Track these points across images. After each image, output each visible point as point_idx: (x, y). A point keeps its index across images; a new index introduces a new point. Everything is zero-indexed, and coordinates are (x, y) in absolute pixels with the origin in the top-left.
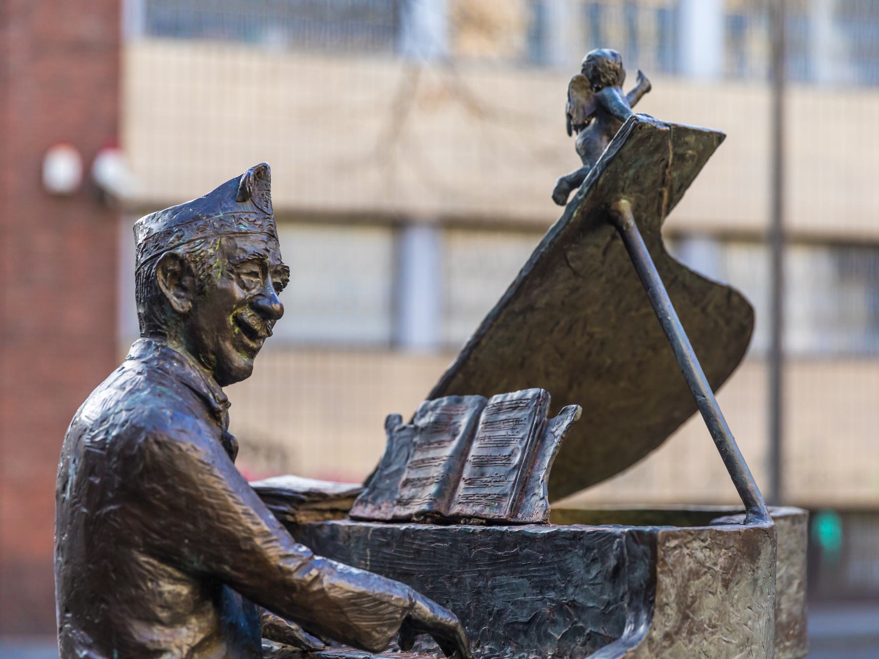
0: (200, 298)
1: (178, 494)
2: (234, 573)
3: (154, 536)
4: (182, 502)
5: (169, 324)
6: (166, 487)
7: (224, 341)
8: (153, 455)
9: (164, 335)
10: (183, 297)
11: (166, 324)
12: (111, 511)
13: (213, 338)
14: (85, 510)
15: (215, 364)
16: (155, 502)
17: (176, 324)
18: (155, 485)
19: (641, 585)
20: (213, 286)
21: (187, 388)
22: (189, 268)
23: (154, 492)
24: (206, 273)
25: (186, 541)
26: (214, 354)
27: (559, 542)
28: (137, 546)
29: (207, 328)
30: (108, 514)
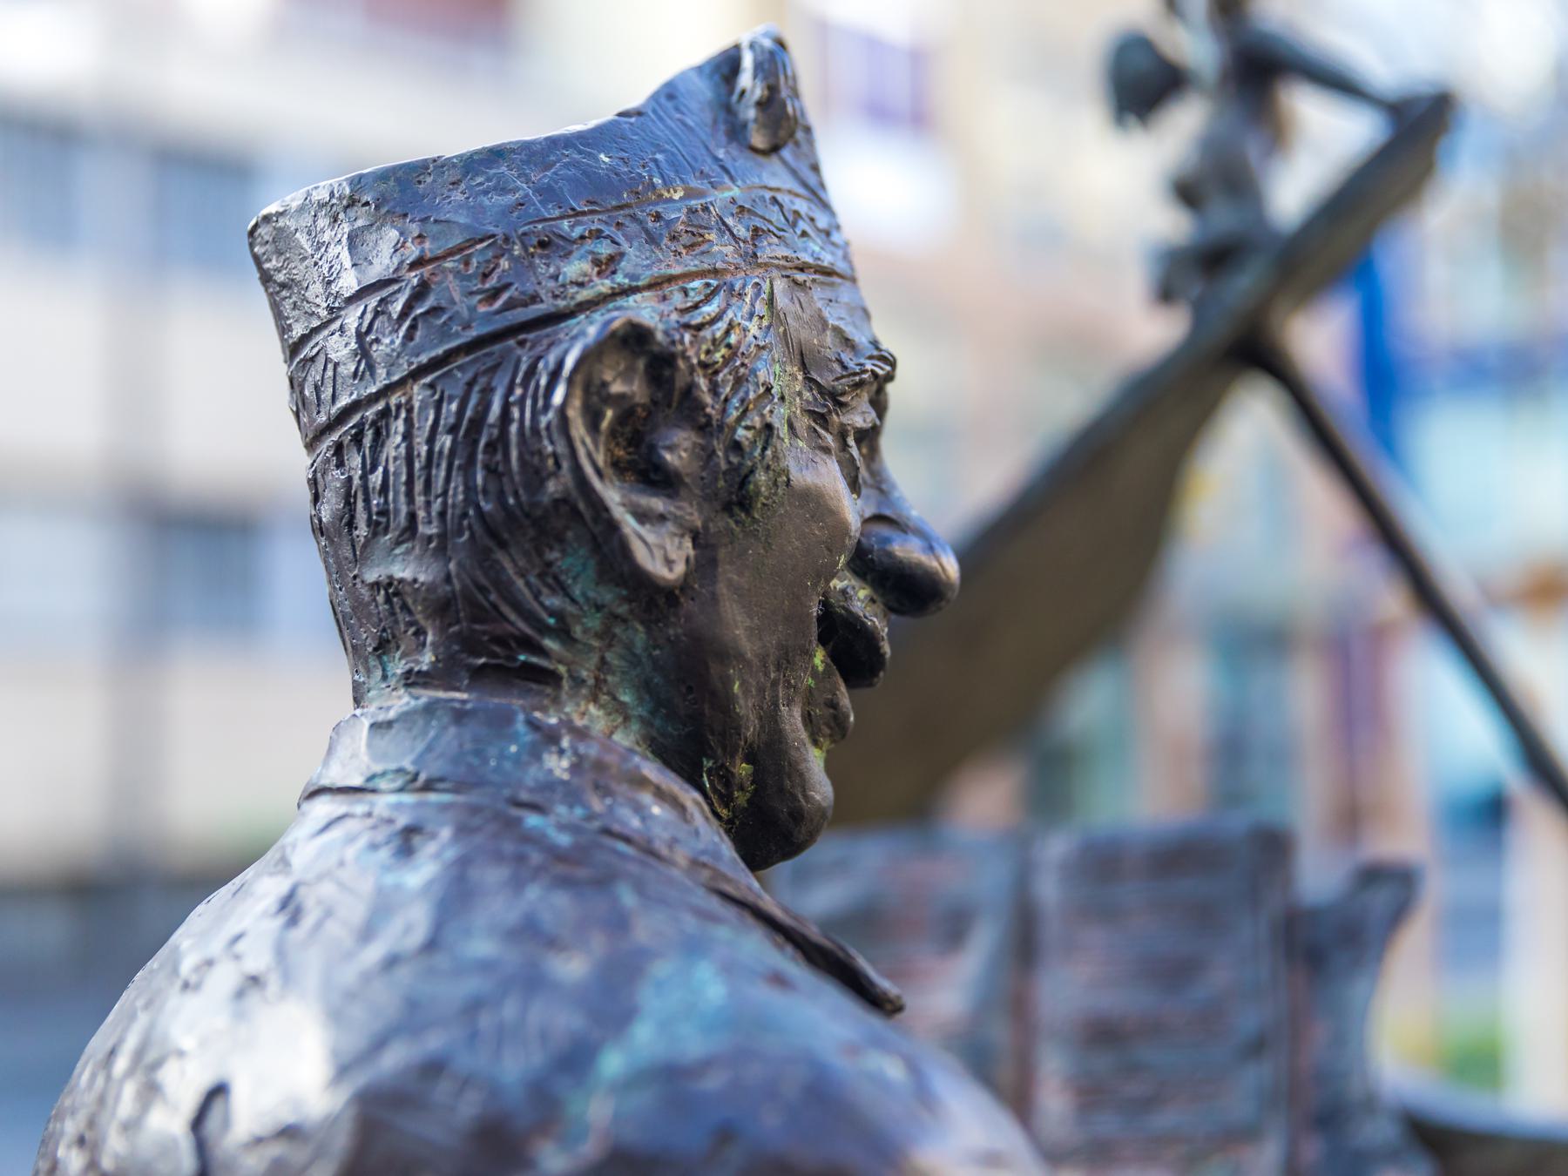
0: (723, 522)
5: (577, 631)
9: (546, 677)
10: (662, 518)
11: (563, 632)
13: (761, 690)
15: (741, 799)
17: (606, 635)
20: (781, 478)
22: (691, 388)
24: (757, 422)
26: (750, 758)
29: (748, 647)
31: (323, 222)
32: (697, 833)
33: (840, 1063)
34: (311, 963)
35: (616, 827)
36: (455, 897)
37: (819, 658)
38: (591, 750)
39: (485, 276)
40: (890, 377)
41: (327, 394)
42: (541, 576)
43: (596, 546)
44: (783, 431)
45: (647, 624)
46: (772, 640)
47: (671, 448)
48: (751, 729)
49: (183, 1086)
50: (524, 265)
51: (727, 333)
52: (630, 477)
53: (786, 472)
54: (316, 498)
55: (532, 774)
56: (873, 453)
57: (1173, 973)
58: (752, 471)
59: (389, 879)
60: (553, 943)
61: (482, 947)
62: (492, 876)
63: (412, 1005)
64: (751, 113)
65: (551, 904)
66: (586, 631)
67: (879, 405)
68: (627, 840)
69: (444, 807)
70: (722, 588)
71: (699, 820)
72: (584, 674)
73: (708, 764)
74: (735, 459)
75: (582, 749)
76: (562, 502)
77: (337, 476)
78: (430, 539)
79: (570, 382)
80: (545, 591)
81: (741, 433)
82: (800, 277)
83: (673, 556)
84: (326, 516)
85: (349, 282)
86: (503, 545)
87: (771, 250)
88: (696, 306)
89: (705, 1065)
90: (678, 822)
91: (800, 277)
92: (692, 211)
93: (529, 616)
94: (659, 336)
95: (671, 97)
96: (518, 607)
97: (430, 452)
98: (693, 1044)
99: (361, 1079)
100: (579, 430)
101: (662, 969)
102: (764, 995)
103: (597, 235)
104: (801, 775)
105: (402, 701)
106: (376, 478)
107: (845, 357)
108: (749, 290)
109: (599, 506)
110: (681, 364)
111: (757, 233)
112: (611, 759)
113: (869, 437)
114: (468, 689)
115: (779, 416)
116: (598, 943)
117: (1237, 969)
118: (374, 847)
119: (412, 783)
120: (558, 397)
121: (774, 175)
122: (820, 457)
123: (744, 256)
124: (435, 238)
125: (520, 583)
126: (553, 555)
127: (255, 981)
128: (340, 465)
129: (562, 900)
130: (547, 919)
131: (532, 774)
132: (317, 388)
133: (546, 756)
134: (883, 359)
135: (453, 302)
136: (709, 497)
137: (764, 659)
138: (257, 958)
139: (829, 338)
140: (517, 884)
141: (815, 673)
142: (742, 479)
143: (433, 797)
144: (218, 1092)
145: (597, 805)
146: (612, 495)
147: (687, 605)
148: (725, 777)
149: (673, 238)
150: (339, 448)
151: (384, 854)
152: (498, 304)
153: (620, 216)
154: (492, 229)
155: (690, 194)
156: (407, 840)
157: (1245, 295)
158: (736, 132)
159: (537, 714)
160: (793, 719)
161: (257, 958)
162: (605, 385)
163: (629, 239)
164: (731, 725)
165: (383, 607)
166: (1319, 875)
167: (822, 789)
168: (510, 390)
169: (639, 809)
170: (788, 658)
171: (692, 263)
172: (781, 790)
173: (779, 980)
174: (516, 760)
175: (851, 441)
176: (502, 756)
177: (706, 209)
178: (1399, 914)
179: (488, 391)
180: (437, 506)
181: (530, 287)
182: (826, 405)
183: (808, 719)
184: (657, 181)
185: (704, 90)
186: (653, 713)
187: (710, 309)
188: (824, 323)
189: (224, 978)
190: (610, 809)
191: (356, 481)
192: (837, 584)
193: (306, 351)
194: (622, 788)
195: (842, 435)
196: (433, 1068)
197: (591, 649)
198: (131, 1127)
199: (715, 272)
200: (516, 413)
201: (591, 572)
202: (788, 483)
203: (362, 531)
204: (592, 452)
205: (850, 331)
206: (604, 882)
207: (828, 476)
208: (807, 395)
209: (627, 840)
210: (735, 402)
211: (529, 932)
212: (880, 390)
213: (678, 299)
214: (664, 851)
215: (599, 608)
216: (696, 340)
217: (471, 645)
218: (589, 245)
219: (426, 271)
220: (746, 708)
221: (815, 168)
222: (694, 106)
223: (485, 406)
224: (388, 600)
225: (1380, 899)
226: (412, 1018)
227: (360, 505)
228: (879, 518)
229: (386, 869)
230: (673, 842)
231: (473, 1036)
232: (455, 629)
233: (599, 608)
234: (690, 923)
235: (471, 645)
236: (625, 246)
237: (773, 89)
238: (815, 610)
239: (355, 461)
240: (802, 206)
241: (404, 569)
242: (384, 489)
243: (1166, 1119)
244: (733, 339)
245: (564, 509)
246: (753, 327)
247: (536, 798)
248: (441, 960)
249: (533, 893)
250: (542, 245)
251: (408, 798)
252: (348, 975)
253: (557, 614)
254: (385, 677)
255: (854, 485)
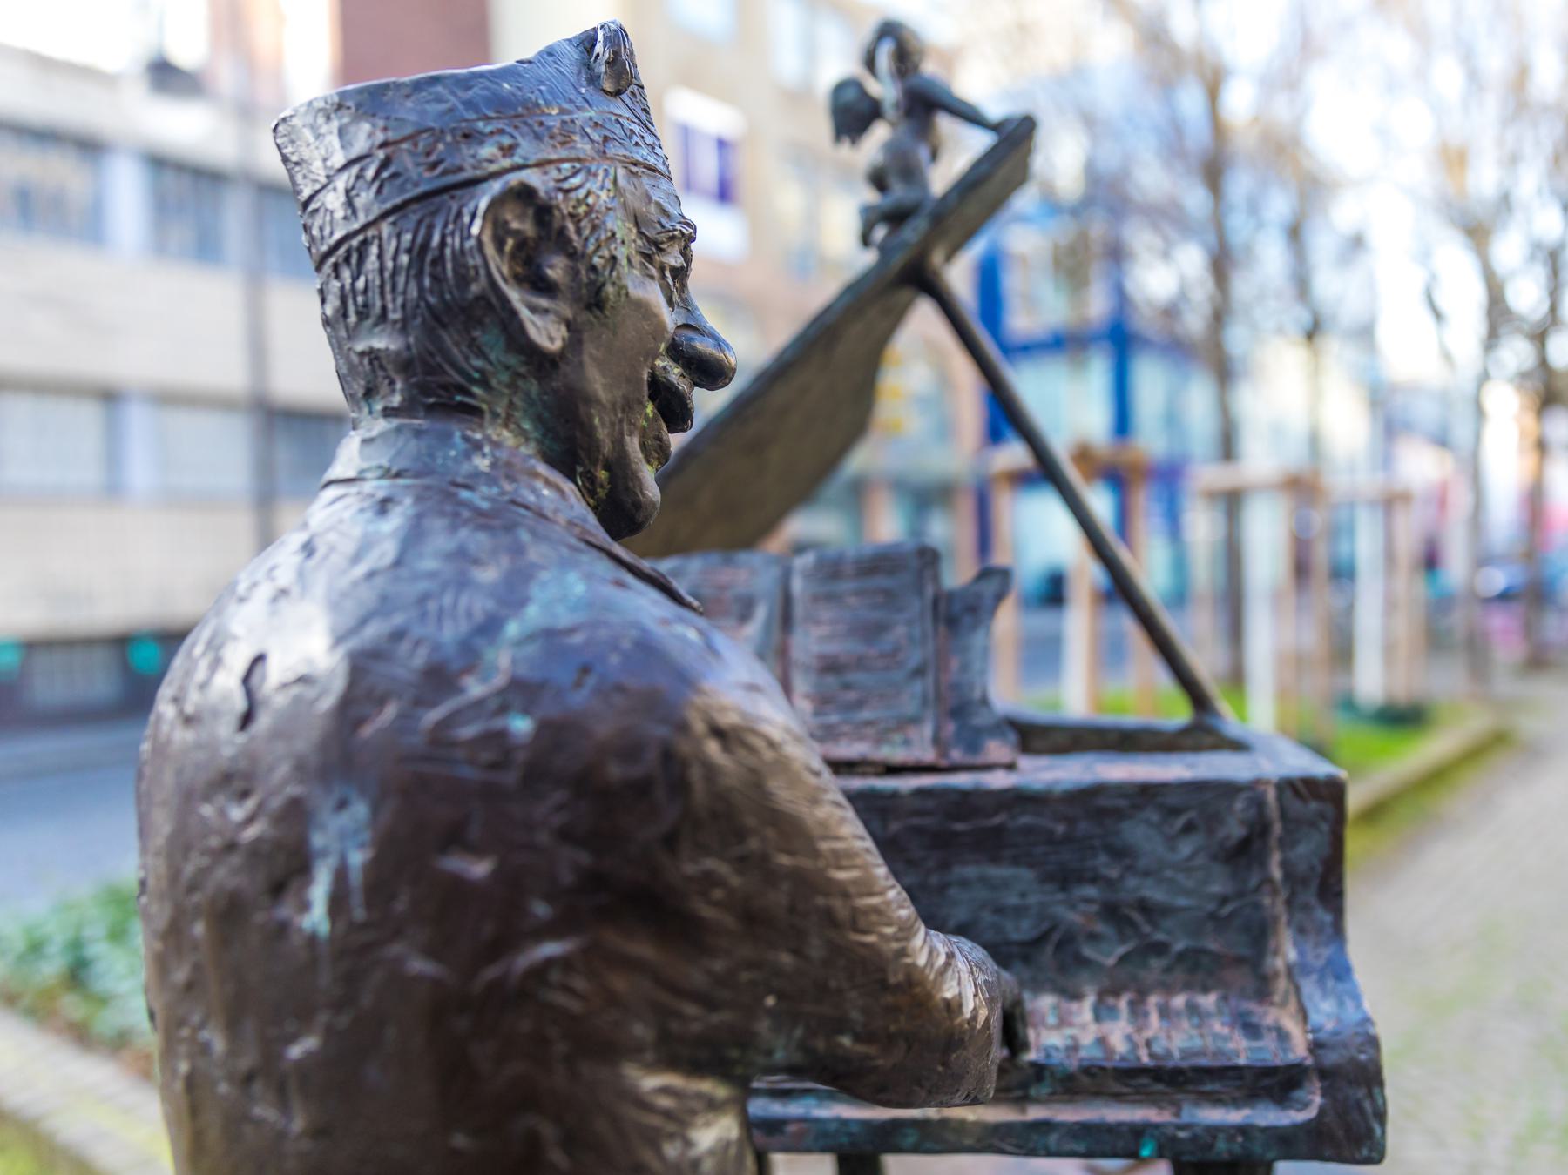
0: (585, 316)
1: (771, 876)
2: (862, 1049)
3: (691, 1009)
4: (778, 898)
5: (494, 382)
6: (742, 863)
7: (630, 435)
8: (710, 770)
10: (546, 311)
11: (484, 383)
12: (549, 962)
13: (613, 424)
14: (419, 965)
15: (602, 493)
16: (707, 912)
17: (512, 386)
18: (710, 864)
19: (1312, 868)
20: (621, 289)
21: (595, 553)
22: (562, 231)
23: (709, 880)
24: (606, 253)
25: (770, 1001)
26: (607, 468)
27: (1103, 802)
28: (634, 1051)
30: (540, 971)
31: (321, 120)
32: (572, 507)
33: (658, 630)
34: (319, 585)
35: (519, 500)
36: (413, 537)
37: (650, 409)
38: (503, 455)
39: (428, 154)
40: (692, 239)
41: (327, 231)
42: (469, 347)
43: (504, 327)
44: (625, 262)
45: (540, 379)
46: (618, 394)
47: (551, 267)
48: (607, 448)
49: (237, 659)
50: (453, 148)
51: (587, 196)
52: (526, 285)
53: (625, 287)
54: (323, 301)
55: (465, 468)
56: (683, 286)
57: (871, 631)
58: (603, 285)
59: (371, 528)
60: (476, 562)
61: (429, 564)
62: (437, 524)
63: (384, 598)
64: (603, 68)
65: (478, 541)
66: (499, 382)
67: (686, 254)
68: (526, 507)
69: (407, 487)
70: (586, 358)
71: (573, 500)
72: (499, 410)
73: (579, 469)
74: (592, 276)
75: (497, 454)
76: (481, 298)
77: (336, 284)
78: (395, 322)
79: (484, 218)
80: (472, 356)
81: (596, 260)
82: (634, 169)
83: (554, 334)
84: (329, 312)
85: (339, 159)
86: (444, 326)
87: (613, 149)
88: (566, 179)
89: (571, 631)
90: (559, 498)
91: (634, 169)
92: (564, 122)
93: (462, 372)
94: (542, 194)
95: (550, 54)
96: (454, 365)
97: (395, 267)
98: (564, 619)
99: (353, 643)
100: (490, 250)
101: (545, 575)
102: (610, 591)
103: (501, 132)
104: (639, 480)
105: (382, 425)
106: (360, 284)
107: (664, 221)
108: (601, 173)
109: (505, 301)
110: (556, 213)
111: (606, 139)
112: (515, 460)
113: (680, 274)
114: (425, 418)
115: (621, 253)
116: (505, 561)
117: (908, 631)
118: (362, 510)
119: (386, 473)
120: (475, 230)
121: (618, 108)
122: (648, 281)
123: (598, 152)
124: (395, 129)
125: (455, 351)
126: (477, 333)
127: (284, 592)
128: (337, 277)
129: (482, 538)
130: (472, 548)
131: (465, 468)
132: (321, 229)
133: (366, 127)
134: (688, 224)
135: (406, 170)
136: (576, 299)
137: (614, 405)
138: (285, 577)
139: (653, 208)
140: (453, 528)
141: (646, 418)
142: (597, 289)
143: (401, 482)
144: (259, 659)
145: (508, 487)
146: (514, 295)
147: (564, 368)
148: (591, 479)
149: (552, 137)
150: (336, 267)
151: (369, 514)
152: (438, 171)
153: (517, 122)
154: (432, 124)
155: (563, 111)
156: (384, 506)
157: (914, 244)
158: (593, 80)
159: (469, 433)
160: (633, 444)
161: (285, 577)
162: (506, 223)
163: (523, 135)
164: (593, 446)
165: (368, 368)
166: (958, 574)
167: (653, 491)
168: (445, 226)
169: (534, 491)
170: (630, 405)
171: (564, 153)
172: (627, 489)
173: (620, 584)
174: (455, 459)
175: (667, 273)
176: (446, 457)
177: (572, 121)
178: (999, 597)
179: (431, 228)
180: (400, 300)
181: (458, 162)
182: (652, 249)
183: (643, 446)
184: (541, 102)
185: (574, 54)
186: (544, 435)
187: (576, 181)
188: (649, 199)
189: (265, 591)
190: (516, 490)
191: (348, 287)
192: (659, 363)
193: (313, 206)
194: (524, 478)
195: (662, 269)
196: (398, 635)
197: (503, 394)
198: (203, 686)
199: (579, 160)
200: (449, 240)
201: (502, 343)
202: (627, 294)
203: (353, 319)
204: (500, 267)
205: (666, 206)
206: (510, 528)
207: (653, 294)
208: (639, 242)
209: (526, 507)
210: (592, 240)
211: (461, 555)
212: (686, 247)
213: (554, 174)
214: (550, 515)
215: (507, 368)
216: (566, 199)
217: (425, 390)
218: (497, 138)
219: (389, 150)
220: (602, 434)
221: (646, 111)
222: (566, 61)
223: (429, 237)
224: (371, 363)
225: (989, 587)
226: (384, 605)
227: (350, 302)
228: (686, 326)
229: (370, 522)
230: (556, 511)
231: (424, 616)
232: (414, 380)
233: (507, 368)
234: (565, 551)
235: (425, 390)
236: (520, 139)
237: (616, 54)
238: (646, 377)
239: (346, 274)
240: (637, 129)
241: (382, 342)
242: (365, 291)
243: (866, 714)
244: (590, 200)
245: (482, 303)
246: (604, 195)
247: (468, 481)
248: (403, 572)
249: (464, 533)
250: (466, 136)
251: (385, 482)
252: (344, 582)
253: (481, 371)
254: (371, 412)
255: (670, 302)
